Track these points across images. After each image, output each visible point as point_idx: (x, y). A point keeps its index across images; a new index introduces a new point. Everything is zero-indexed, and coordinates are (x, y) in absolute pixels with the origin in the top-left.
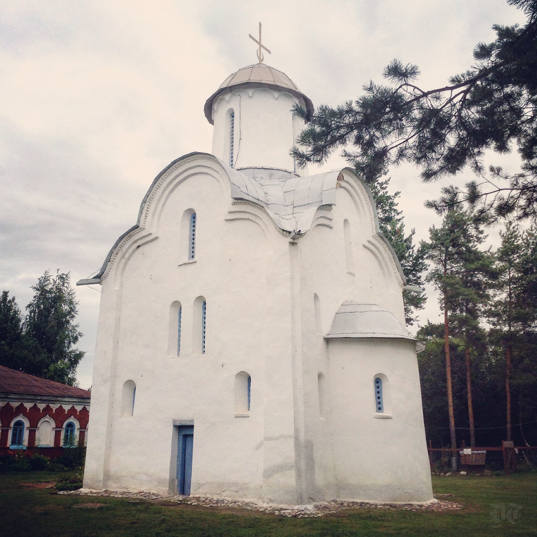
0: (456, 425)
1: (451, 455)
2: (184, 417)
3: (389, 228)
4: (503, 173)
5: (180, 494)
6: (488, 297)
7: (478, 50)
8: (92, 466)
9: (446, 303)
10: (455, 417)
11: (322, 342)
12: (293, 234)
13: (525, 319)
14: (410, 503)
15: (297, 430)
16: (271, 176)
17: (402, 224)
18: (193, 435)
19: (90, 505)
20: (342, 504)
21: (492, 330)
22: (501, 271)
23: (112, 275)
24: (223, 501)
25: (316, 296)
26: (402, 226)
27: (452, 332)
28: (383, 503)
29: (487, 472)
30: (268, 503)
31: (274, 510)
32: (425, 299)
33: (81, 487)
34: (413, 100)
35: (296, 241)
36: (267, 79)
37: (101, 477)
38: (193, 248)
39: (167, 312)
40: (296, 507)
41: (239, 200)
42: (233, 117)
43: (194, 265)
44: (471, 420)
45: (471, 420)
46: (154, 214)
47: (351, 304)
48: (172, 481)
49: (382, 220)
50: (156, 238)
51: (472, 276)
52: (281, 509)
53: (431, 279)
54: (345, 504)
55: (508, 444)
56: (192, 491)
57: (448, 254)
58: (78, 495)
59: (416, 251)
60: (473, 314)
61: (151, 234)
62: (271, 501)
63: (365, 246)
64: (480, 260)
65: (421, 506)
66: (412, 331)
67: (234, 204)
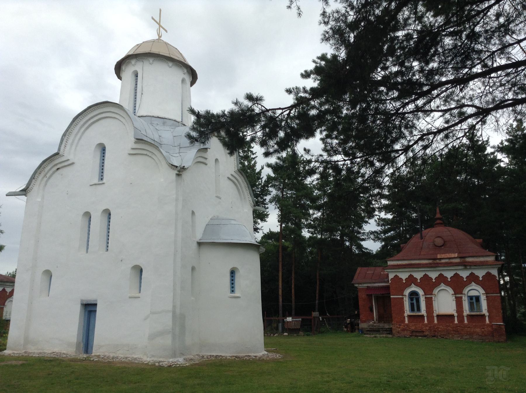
0: (283, 301)
1: (279, 322)
2: (90, 298)
3: (246, 163)
4: (311, 153)
5: (85, 353)
6: (309, 215)
7: (304, 73)
8: (14, 334)
9: (281, 218)
10: (282, 296)
11: (195, 244)
12: (179, 168)
13: (332, 231)
14: (250, 354)
15: (174, 307)
16: (164, 124)
17: (255, 162)
18: (96, 311)
19: (14, 363)
20: (203, 357)
21: (310, 237)
22: (318, 198)
23: (35, 188)
24: (117, 358)
25: (193, 213)
26: (255, 163)
27: (284, 237)
28: (235, 355)
29: (301, 333)
30: (150, 358)
31: (155, 362)
32: (268, 215)
33: (5, 349)
34: (261, 113)
35: (181, 173)
36: (164, 52)
37: (22, 342)
38: (102, 172)
39: (79, 220)
40: (171, 360)
41: (139, 140)
42: (137, 76)
43: (103, 185)
44: (293, 297)
45: (293, 297)
46: (72, 144)
47: (218, 218)
48: (78, 344)
49: (242, 157)
50: (73, 163)
51: (300, 200)
52: (160, 362)
53: (273, 202)
54: (205, 357)
55: (315, 314)
56: (94, 351)
57: (284, 183)
58: (4, 355)
59: (263, 181)
60: (299, 227)
61: (68, 160)
62: (153, 356)
63: (228, 178)
64: (305, 189)
65: (256, 357)
66: (259, 236)
67: (135, 143)
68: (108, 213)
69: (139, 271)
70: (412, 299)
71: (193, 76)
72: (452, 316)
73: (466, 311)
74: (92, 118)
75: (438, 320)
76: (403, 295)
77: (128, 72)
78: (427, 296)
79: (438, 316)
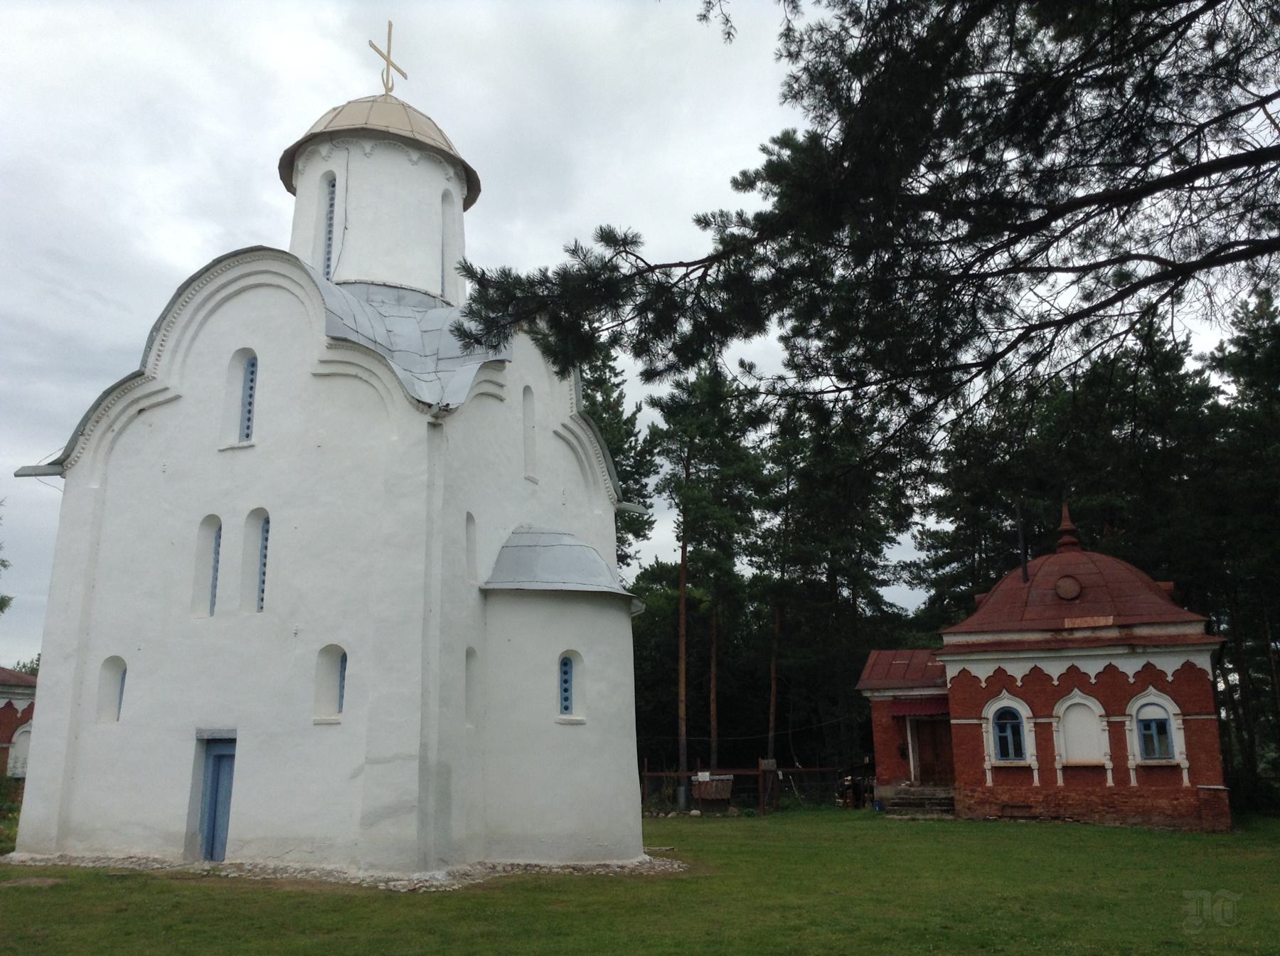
0: (688, 733)
1: (678, 783)
2: (218, 724)
3: (599, 397)
4: (757, 371)
5: (206, 858)
6: (753, 524)
7: (739, 178)
8: (35, 811)
9: (684, 531)
10: (687, 720)
11: (475, 594)
12: (435, 410)
13: (807, 561)
14: (608, 862)
15: (424, 746)
16: (399, 300)
17: (621, 393)
18: (233, 757)
19: (34, 882)
20: (494, 867)
21: (755, 576)
22: (775, 481)
23: (86, 458)
24: (285, 870)
25: (470, 518)
26: (621, 396)
27: (691, 577)
29: (733, 810)
30: (366, 870)
31: (377, 881)
32: (653, 522)
33: (13, 849)
34: (635, 274)
35: (440, 421)
36: (398, 126)
37: (54, 832)
38: (249, 419)
39: (193, 534)
40: (416, 876)
41: (338, 342)
42: (334, 186)
43: (250, 451)
44: (714, 723)
45: (714, 723)
46: (175, 351)
47: (529, 531)
48: (190, 838)
49: (588, 383)
50: (177, 398)
51: (730, 486)
52: (389, 880)
53: (664, 491)
54: (499, 868)
55: (768, 764)
56: (228, 853)
57: (691, 445)
58: (9, 864)
59: (641, 441)
60: (728, 553)
61: (166, 389)
62: (372, 866)
63: (556, 433)
64: (742, 460)
65: (622, 867)
66: (630, 574)
67: (330, 347)
68: (262, 519)
69: (339, 658)
70: (1001, 728)
71: (470, 184)
72: (1100, 769)
73: (1135, 755)
74: (224, 286)
75: (1065, 779)
76: (981, 719)
77: (311, 175)
78: (1040, 720)
79: (1066, 769)
